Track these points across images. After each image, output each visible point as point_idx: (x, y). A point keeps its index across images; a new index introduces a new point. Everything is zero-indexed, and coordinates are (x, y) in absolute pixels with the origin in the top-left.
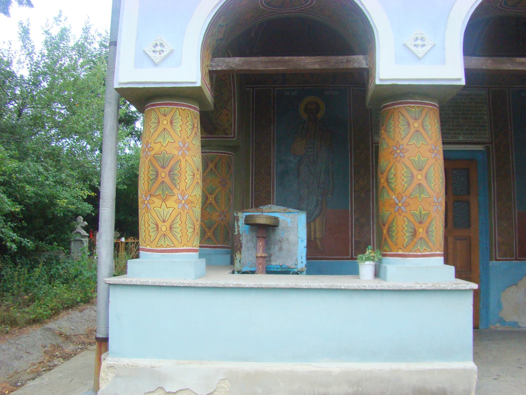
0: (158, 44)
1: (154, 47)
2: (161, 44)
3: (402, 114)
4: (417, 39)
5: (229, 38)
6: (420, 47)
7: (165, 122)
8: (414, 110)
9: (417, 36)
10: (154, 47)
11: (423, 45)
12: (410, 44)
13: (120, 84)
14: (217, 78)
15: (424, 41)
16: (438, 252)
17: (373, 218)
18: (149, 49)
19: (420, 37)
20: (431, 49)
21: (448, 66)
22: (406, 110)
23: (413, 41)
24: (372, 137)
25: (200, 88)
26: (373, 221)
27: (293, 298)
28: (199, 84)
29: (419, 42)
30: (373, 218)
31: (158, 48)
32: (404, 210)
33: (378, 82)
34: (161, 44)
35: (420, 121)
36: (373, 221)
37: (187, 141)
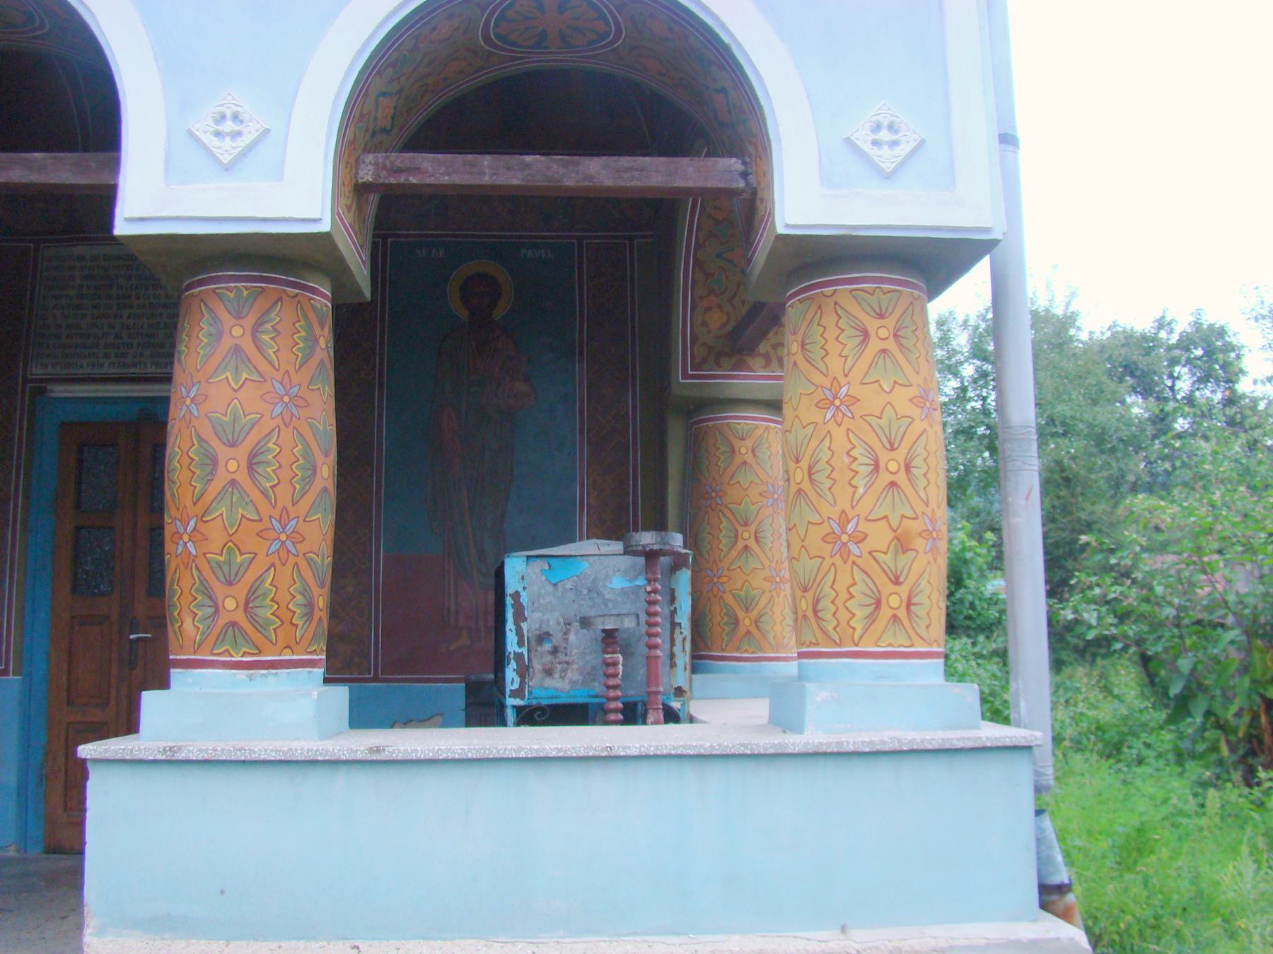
0: (229, 114)
1: (217, 122)
2: (236, 117)
3: (206, 305)
4: (877, 127)
5: (420, 106)
6: (886, 148)
7: (237, 331)
8: (232, 295)
9: (222, 109)
10: (217, 122)
11: (894, 144)
12: (863, 140)
13: (788, 226)
14: (388, 213)
15: (896, 132)
16: (935, 649)
17: (12, 570)
18: (203, 127)
19: (229, 114)
20: (914, 152)
21: (293, 183)
22: (220, 297)
23: (210, 122)
24: (26, 364)
25: (325, 238)
26: (11, 576)
27: (602, 782)
28: (325, 227)
29: (884, 135)
30: (12, 570)
31: (229, 126)
32: (293, 550)
33: (781, 230)
34: (236, 117)
35: (249, 321)
36: (11, 576)
37: (296, 379)
